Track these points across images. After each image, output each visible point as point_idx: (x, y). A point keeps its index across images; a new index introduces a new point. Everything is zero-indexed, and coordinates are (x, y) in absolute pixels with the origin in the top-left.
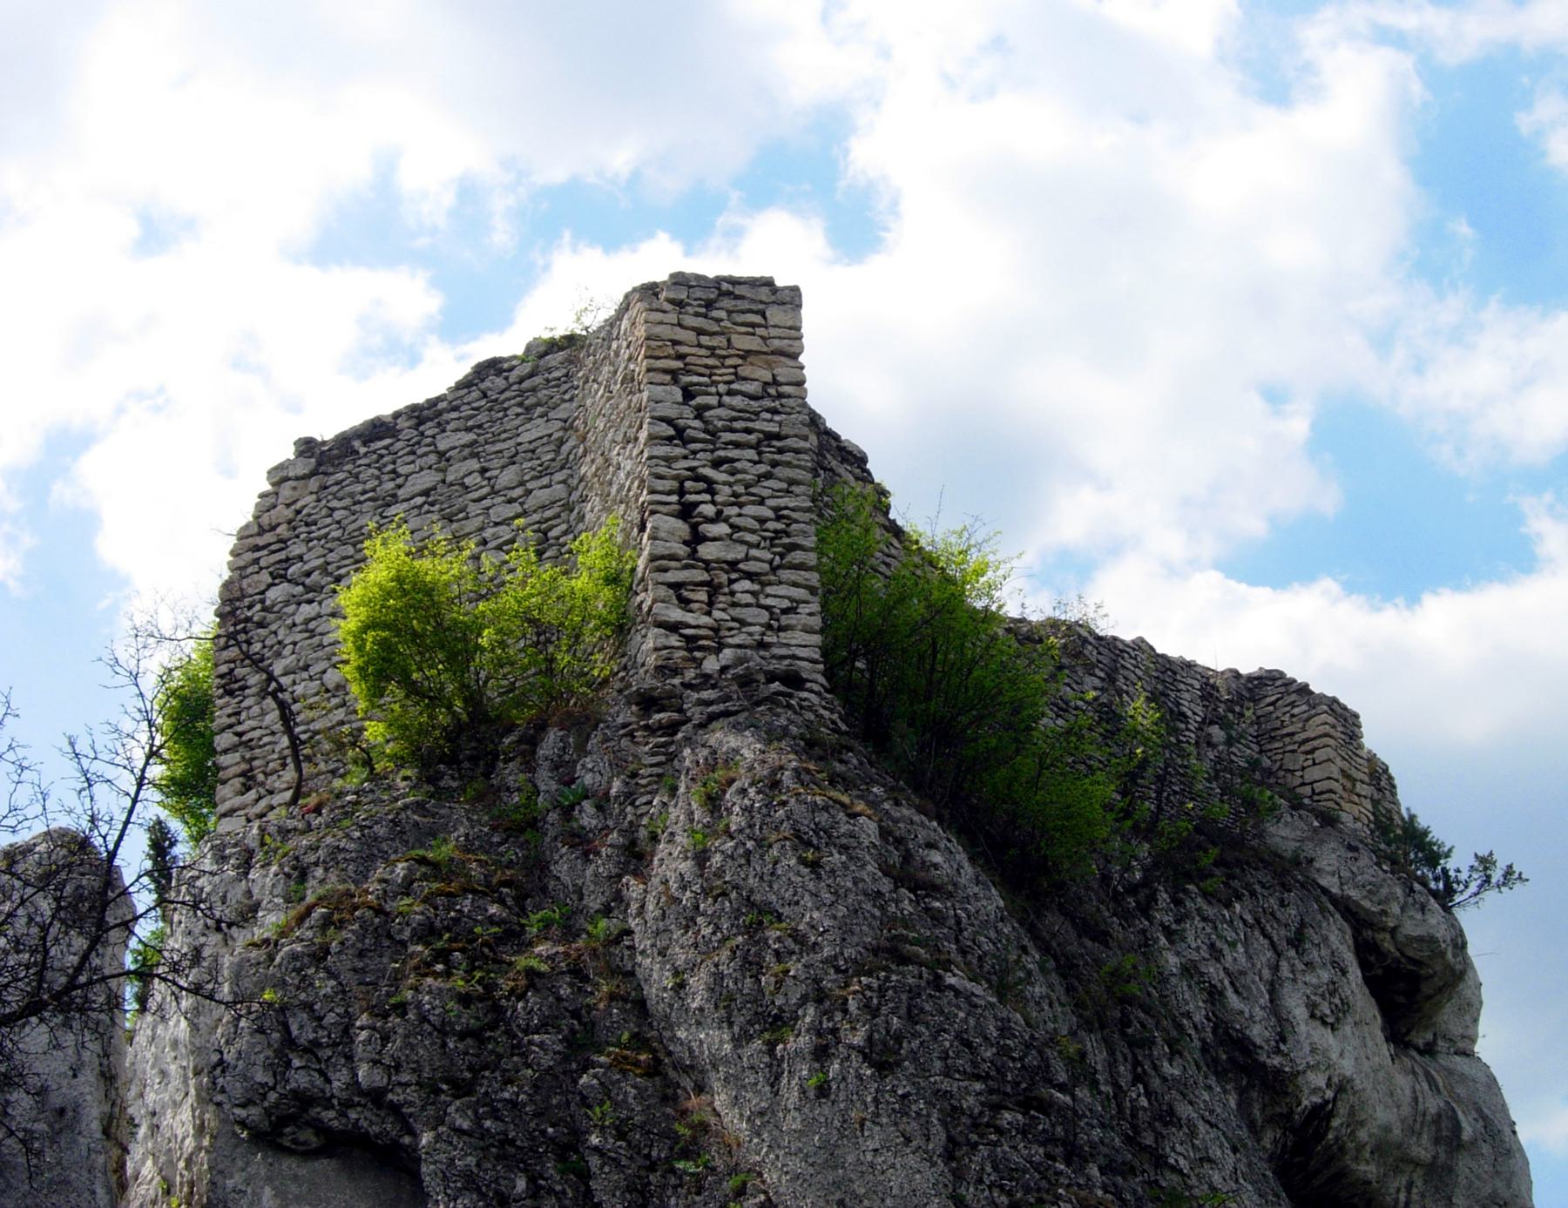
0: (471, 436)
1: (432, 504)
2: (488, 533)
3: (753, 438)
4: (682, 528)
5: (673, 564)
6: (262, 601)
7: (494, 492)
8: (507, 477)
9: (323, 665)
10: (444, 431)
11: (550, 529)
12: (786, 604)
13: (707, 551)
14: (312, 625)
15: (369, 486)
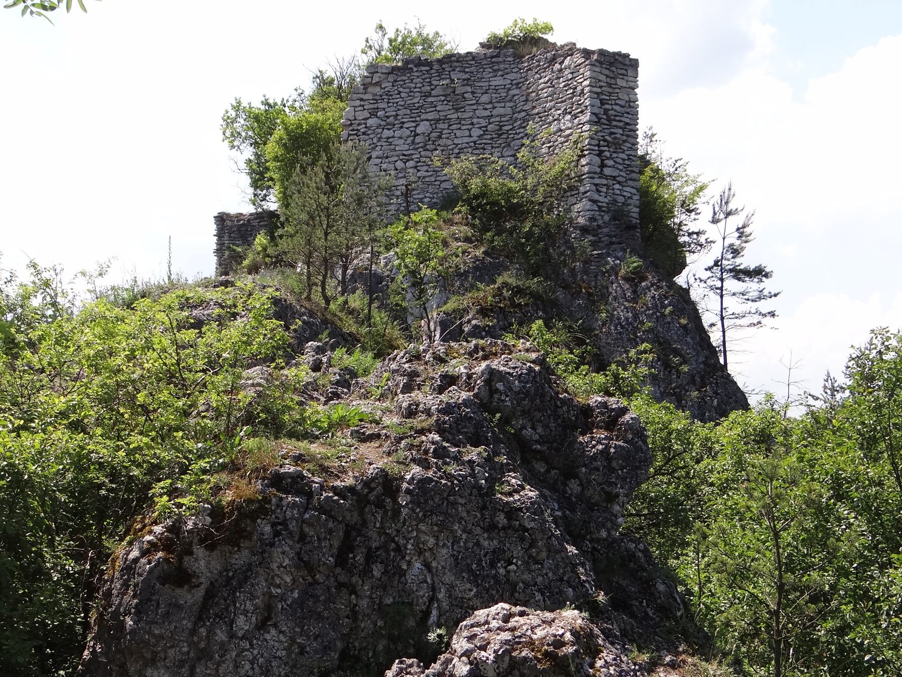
0: (467, 76)
1: (449, 101)
2: (475, 121)
3: (621, 124)
4: (597, 160)
5: (596, 176)
6: (365, 124)
7: (477, 103)
8: (485, 98)
9: (396, 158)
10: (454, 70)
11: (504, 126)
12: (629, 195)
13: (607, 171)
14: (390, 140)
15: (418, 85)
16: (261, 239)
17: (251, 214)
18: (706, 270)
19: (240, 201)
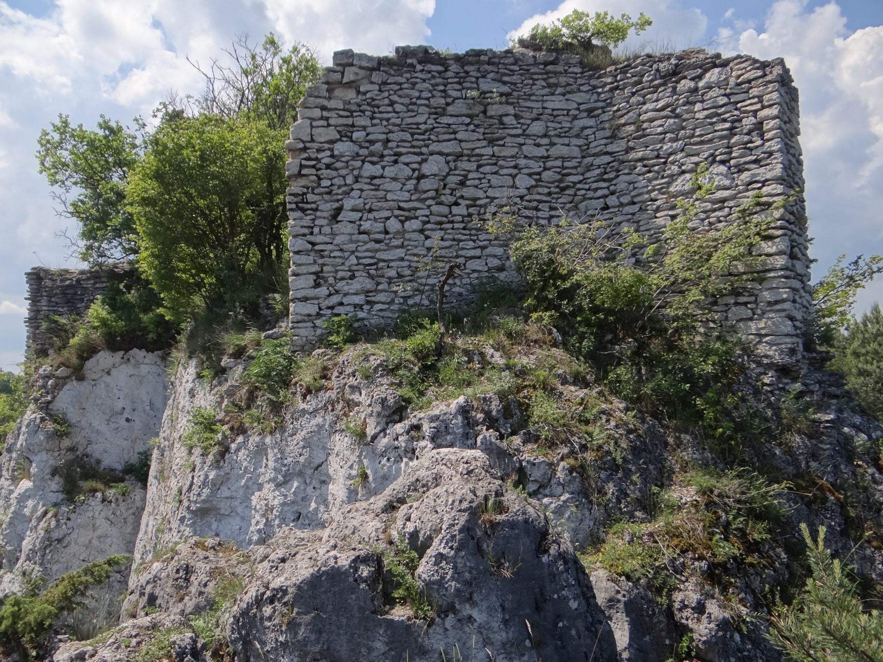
16: (97, 310)
17: (82, 272)
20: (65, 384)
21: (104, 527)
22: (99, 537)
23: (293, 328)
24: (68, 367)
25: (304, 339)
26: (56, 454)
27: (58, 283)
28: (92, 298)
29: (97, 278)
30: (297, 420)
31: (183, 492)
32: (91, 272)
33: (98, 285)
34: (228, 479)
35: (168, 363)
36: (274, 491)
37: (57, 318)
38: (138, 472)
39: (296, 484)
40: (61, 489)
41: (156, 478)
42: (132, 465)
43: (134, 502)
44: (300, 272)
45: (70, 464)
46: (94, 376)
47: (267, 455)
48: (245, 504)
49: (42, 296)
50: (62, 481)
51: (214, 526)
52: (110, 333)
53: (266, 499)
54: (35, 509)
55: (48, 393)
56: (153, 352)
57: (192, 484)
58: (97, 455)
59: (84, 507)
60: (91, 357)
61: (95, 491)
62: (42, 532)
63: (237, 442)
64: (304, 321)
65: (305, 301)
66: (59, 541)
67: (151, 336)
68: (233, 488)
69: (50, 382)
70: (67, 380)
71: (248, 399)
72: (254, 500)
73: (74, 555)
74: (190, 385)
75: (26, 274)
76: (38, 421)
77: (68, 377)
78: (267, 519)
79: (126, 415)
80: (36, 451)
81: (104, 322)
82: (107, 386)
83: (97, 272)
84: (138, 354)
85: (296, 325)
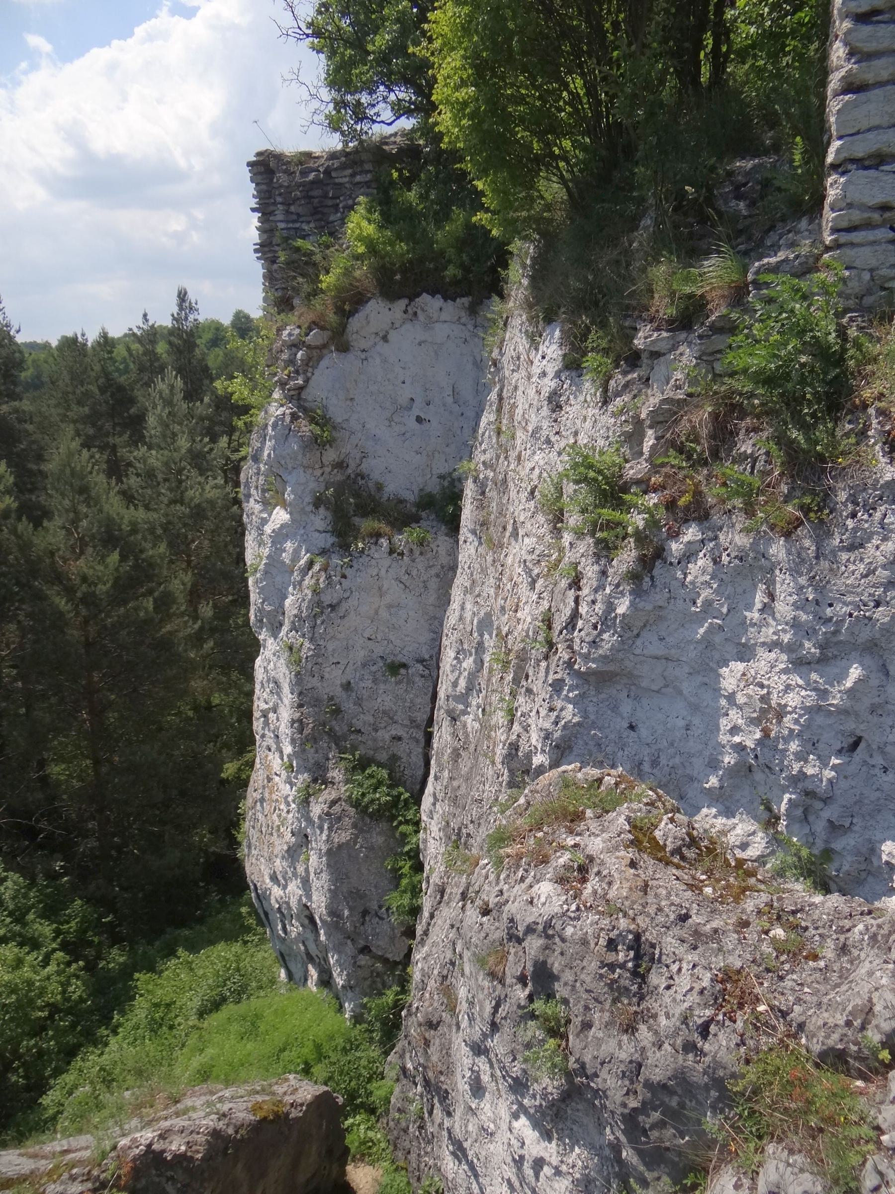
16: (360, 224)
17: (333, 156)
18: (182, 296)
19: (302, 125)
20: (320, 358)
21: (394, 593)
22: (389, 607)
23: (837, 245)
24: (322, 328)
25: (866, 276)
26: (318, 472)
27: (298, 178)
28: (350, 202)
29: (355, 163)
30: (870, 509)
31: (557, 626)
32: (347, 154)
33: (358, 178)
34: (661, 618)
35: (479, 320)
36: (785, 671)
37: (299, 242)
38: (441, 508)
39: (855, 672)
40: (329, 528)
41: (474, 532)
42: (430, 496)
43: (436, 557)
44: (870, 77)
45: (340, 488)
46: (363, 344)
47: (770, 584)
48: (700, 679)
49: (275, 204)
50: (329, 515)
51: (626, 707)
52: (383, 266)
53: (762, 686)
54: (296, 557)
55: (297, 372)
56: (454, 300)
57: (575, 615)
58: (376, 476)
59: (364, 559)
60: (356, 311)
61: (378, 535)
62: (309, 593)
63: (686, 539)
64: (868, 225)
65: (876, 167)
66: (333, 607)
67: (451, 271)
68: (670, 640)
69: (299, 355)
70: (325, 351)
71: (713, 436)
72: (731, 676)
73: (356, 630)
74: (549, 384)
75: (249, 164)
76: (288, 419)
77: (324, 346)
78: (766, 733)
79: (416, 412)
80: (290, 466)
81: (372, 247)
82: (385, 361)
83: (356, 151)
84: (430, 303)
85: (844, 238)
